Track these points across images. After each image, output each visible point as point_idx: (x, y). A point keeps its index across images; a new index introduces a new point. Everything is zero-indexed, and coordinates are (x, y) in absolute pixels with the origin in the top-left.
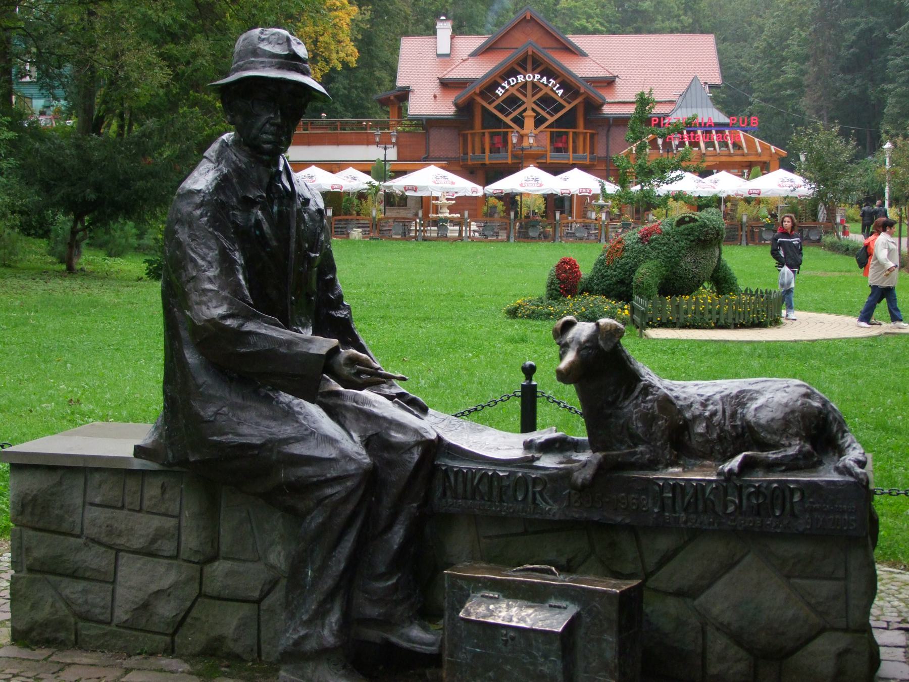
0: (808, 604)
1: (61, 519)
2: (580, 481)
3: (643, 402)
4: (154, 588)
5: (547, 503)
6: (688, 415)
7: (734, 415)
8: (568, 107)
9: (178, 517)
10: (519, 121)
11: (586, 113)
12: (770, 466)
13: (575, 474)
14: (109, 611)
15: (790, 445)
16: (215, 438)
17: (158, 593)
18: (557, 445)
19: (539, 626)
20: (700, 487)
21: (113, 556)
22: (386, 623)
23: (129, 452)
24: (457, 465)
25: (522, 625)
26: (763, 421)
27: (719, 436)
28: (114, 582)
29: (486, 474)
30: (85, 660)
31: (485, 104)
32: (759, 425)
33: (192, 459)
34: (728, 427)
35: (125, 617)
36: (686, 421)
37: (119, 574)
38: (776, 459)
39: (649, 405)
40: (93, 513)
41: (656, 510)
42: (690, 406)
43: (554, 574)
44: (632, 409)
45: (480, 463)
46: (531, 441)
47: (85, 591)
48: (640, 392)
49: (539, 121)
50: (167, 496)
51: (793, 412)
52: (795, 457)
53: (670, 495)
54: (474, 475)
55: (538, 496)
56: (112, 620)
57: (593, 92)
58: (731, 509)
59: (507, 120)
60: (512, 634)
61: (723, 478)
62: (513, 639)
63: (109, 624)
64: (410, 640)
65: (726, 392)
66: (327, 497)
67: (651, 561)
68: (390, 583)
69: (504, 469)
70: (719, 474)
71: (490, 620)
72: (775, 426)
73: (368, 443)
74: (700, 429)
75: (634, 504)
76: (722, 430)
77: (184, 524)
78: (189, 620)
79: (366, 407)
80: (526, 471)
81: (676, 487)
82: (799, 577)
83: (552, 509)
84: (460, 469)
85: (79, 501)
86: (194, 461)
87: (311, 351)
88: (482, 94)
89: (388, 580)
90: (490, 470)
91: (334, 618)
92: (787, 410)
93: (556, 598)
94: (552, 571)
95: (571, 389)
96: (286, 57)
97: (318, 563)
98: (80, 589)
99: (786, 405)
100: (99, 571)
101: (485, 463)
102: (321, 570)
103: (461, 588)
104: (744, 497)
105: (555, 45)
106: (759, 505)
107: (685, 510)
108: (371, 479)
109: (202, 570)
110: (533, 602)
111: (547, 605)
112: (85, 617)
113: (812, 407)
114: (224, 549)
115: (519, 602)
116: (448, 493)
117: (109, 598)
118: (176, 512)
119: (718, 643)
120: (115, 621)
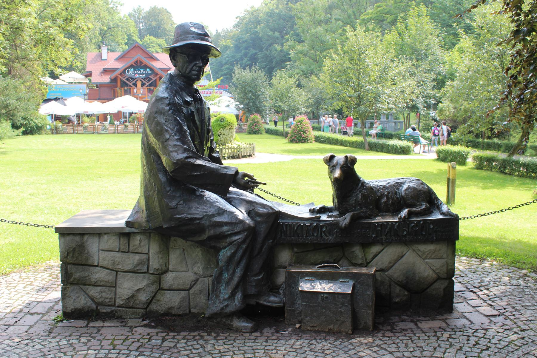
0: (433, 270)
1: (87, 259)
2: (343, 225)
4: (137, 288)
5: (327, 236)
8: (154, 79)
10: (135, 85)
12: (418, 214)
13: (341, 223)
14: (113, 300)
15: (421, 205)
16: (177, 216)
19: (339, 291)
21: (115, 274)
22: (259, 295)
23: (124, 225)
24: (286, 221)
25: (330, 291)
28: (115, 287)
31: (122, 78)
33: (165, 227)
37: (118, 282)
40: (103, 255)
41: (374, 236)
43: (338, 268)
45: (296, 220)
46: (314, 209)
47: (101, 292)
49: (143, 85)
50: (142, 244)
54: (294, 226)
55: (323, 234)
56: (115, 304)
58: (405, 233)
59: (131, 84)
60: (326, 295)
62: (326, 298)
63: (114, 306)
64: (269, 302)
66: (235, 241)
68: (260, 277)
71: (314, 290)
73: (249, 213)
74: (384, 200)
77: (151, 257)
78: (154, 301)
79: (245, 198)
81: (383, 225)
82: (429, 259)
83: (330, 239)
84: (288, 224)
86: (167, 228)
87: (228, 173)
88: (120, 74)
89: (259, 276)
91: (239, 296)
97: (231, 271)
98: (99, 291)
100: (108, 282)
101: (298, 220)
103: (295, 277)
104: (410, 228)
105: (147, 56)
107: (386, 235)
109: (160, 279)
111: (339, 281)
114: (171, 267)
115: (325, 281)
118: (147, 252)
120: (117, 305)
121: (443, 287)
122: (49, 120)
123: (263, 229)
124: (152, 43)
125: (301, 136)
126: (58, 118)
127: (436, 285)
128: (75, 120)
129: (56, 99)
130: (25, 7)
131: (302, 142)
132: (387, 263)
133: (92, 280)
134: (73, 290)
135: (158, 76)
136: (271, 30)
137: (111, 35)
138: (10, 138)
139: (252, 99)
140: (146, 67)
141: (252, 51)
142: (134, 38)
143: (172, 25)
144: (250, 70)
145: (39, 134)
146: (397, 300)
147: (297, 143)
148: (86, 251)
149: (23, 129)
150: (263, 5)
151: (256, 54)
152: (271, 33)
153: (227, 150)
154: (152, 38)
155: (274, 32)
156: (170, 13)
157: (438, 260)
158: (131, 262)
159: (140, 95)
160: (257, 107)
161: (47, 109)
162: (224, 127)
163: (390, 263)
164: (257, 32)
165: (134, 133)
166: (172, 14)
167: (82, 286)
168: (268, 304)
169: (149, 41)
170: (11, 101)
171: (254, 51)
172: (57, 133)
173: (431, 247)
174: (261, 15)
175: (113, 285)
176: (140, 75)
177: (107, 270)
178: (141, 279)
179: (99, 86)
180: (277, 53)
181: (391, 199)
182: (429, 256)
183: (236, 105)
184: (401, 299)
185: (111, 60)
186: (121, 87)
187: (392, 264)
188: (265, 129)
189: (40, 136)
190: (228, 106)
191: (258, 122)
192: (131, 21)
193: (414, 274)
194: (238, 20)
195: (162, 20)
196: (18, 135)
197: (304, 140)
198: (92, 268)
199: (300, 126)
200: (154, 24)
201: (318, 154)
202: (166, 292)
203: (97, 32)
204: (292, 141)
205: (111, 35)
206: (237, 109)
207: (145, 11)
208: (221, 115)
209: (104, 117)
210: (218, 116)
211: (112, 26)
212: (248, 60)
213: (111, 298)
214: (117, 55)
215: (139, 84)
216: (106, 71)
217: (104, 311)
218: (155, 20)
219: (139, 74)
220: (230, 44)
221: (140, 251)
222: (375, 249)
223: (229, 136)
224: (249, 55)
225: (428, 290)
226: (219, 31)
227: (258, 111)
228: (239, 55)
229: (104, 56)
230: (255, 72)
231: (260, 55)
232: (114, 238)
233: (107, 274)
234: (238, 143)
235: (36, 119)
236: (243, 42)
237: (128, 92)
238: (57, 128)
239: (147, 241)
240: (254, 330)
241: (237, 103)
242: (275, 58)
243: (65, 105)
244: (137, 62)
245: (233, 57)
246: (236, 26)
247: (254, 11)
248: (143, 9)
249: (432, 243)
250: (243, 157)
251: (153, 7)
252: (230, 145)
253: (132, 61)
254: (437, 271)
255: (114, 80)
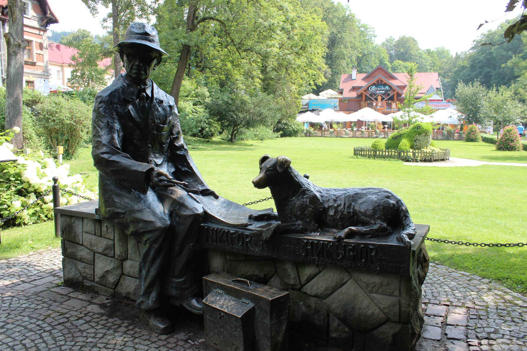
1: (75, 238)
3: (302, 198)
5: (253, 247)
6: (326, 206)
7: (349, 207)
8: (391, 95)
9: (114, 240)
10: (376, 99)
11: (397, 97)
15: (375, 224)
17: (107, 272)
18: (266, 217)
20: (325, 244)
24: (215, 226)
26: (362, 210)
27: (340, 217)
29: (225, 231)
30: (81, 297)
32: (360, 212)
34: (345, 212)
35: (98, 280)
36: (324, 208)
38: (366, 231)
39: (305, 200)
40: (85, 236)
42: (328, 201)
44: (297, 202)
48: (301, 193)
49: (382, 99)
50: (109, 231)
51: (379, 206)
52: (377, 231)
53: (310, 247)
57: (399, 91)
59: (373, 99)
60: (222, 314)
61: (336, 240)
62: (223, 316)
65: (349, 194)
67: (304, 279)
69: (233, 229)
70: (335, 238)
72: (368, 213)
75: (293, 251)
76: (342, 214)
80: (243, 231)
81: (316, 244)
83: (257, 251)
85: (81, 231)
88: (365, 91)
89: (181, 278)
90: (226, 228)
91: (153, 295)
92: (376, 205)
93: (245, 298)
94: (247, 282)
95: (267, 191)
96: (142, 34)
99: (376, 202)
102: (148, 272)
104: (347, 251)
106: (354, 256)
107: (318, 256)
108: (169, 233)
110: (236, 298)
112: (85, 278)
113: (389, 203)
115: (230, 297)
116: (209, 239)
117: (92, 271)
119: (335, 323)
121: (392, 331)
122: (306, 127)
123: (182, 230)
124: (400, 66)
125: (509, 145)
126: (312, 125)
127: (385, 328)
128: (325, 126)
129: (313, 111)
130: (271, 40)
131: (509, 150)
132: (323, 289)
133: (78, 257)
134: (68, 263)
135: (395, 92)
136: (505, 50)
137: (367, 61)
138: (271, 138)
139: (473, 111)
140: (385, 85)
141: (486, 70)
142: (385, 62)
143: (417, 50)
144: (473, 86)
145: (295, 136)
146: (334, 336)
147: (504, 150)
148: (74, 231)
149: (281, 132)
150: (500, 28)
151: (489, 72)
152: (504, 53)
153: (420, 154)
154: (400, 62)
155: (508, 52)
156: (416, 41)
157: (387, 297)
158: (101, 246)
159: (378, 107)
160: (477, 118)
161: (301, 118)
162: (420, 134)
163: (326, 289)
164: (492, 53)
165: (368, 137)
166: (418, 42)
167: (73, 260)
168: (187, 307)
169: (397, 64)
170: (263, 111)
171: (488, 70)
172: (309, 136)
173: (376, 280)
174: (496, 37)
175: (93, 263)
176: (381, 91)
177: (88, 250)
178: (109, 262)
179: (350, 100)
180: (509, 71)
181: (346, 213)
182: (375, 289)
183: (458, 116)
184: (340, 335)
185: (358, 80)
186: (366, 100)
187: (329, 292)
188: (482, 137)
189: (296, 138)
190: (451, 117)
191: (475, 131)
192: (384, 50)
193: (353, 309)
194: (475, 43)
195: (409, 47)
196: (277, 137)
197: (512, 149)
198: (79, 246)
199: (508, 135)
200: (402, 50)
201: (515, 161)
202: (127, 277)
203: (354, 59)
204: (500, 149)
205: (367, 61)
206: (459, 120)
207: (395, 40)
208: (418, 123)
209: (346, 125)
210: (415, 124)
211: (366, 53)
212: (482, 78)
213: (91, 275)
214: (364, 75)
215: (379, 98)
216: (354, 89)
217: (87, 284)
218: (403, 47)
219: (379, 90)
220: (466, 64)
221: (108, 237)
222: (308, 271)
223: (425, 141)
224: (483, 73)
225: (374, 332)
226: (459, 54)
227: (478, 121)
228: (474, 74)
229: (354, 77)
230: (477, 87)
231: (493, 73)
232: (90, 222)
233: (87, 253)
234: (432, 148)
235: (294, 125)
236: (479, 62)
237: (370, 106)
238: (310, 133)
239: (112, 228)
240: (165, 332)
241: (460, 114)
242: (507, 75)
243: (319, 115)
244: (378, 81)
245: (469, 75)
246: (472, 48)
247: (490, 34)
248: (394, 39)
249: (378, 275)
250: (435, 161)
251: (402, 36)
252: (425, 150)
253: (374, 80)
254: (385, 311)
255: (360, 96)
